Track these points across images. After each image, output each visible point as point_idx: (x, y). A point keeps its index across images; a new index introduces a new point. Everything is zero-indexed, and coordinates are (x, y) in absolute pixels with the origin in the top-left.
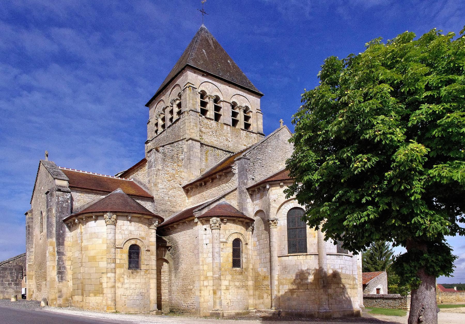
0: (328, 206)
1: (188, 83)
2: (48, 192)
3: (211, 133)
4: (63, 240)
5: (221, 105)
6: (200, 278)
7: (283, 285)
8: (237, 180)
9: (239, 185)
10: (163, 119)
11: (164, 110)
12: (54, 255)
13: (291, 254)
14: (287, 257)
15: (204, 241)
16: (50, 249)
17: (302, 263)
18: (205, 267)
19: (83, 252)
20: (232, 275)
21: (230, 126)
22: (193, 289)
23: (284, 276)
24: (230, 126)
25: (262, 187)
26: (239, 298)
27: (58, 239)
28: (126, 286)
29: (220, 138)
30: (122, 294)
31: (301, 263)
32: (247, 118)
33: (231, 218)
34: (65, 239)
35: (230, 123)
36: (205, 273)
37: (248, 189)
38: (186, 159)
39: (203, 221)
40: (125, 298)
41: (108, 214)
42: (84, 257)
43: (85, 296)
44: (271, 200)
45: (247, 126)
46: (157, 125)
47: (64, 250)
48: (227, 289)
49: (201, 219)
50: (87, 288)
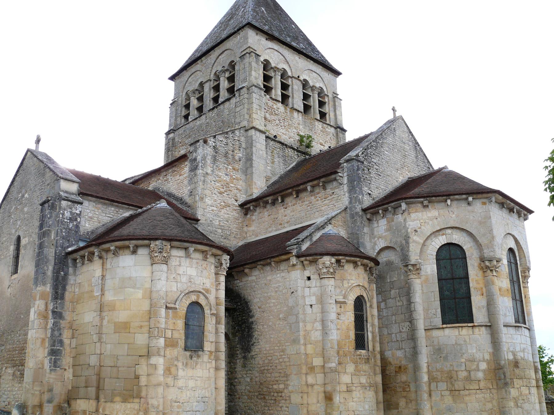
0: (297, 248)
1: (249, 47)
2: (47, 201)
3: (277, 122)
4: (64, 289)
5: (289, 82)
6: (301, 369)
7: (437, 382)
8: (347, 195)
9: (350, 202)
10: (201, 99)
11: (202, 85)
12: (46, 317)
13: (448, 326)
14: (442, 331)
15: (307, 299)
16: (38, 305)
17: (468, 340)
18: (310, 349)
19: (104, 314)
20: (355, 363)
21: (302, 112)
22: (285, 391)
23: (439, 366)
24: (302, 112)
25: (392, 207)
26: (367, 407)
27: (55, 288)
28: (181, 383)
29: (290, 131)
30: (174, 399)
31: (465, 341)
32: (322, 104)
33: (353, 259)
34: (67, 287)
35: (301, 108)
36: (309, 360)
37: (365, 210)
38: (243, 160)
39: (305, 262)
40: (179, 407)
41: (158, 242)
42: (105, 322)
43: (102, 400)
44: (409, 230)
45: (323, 115)
46: (187, 106)
47: (63, 308)
48: (349, 391)
49: (302, 259)
50: (108, 384)
